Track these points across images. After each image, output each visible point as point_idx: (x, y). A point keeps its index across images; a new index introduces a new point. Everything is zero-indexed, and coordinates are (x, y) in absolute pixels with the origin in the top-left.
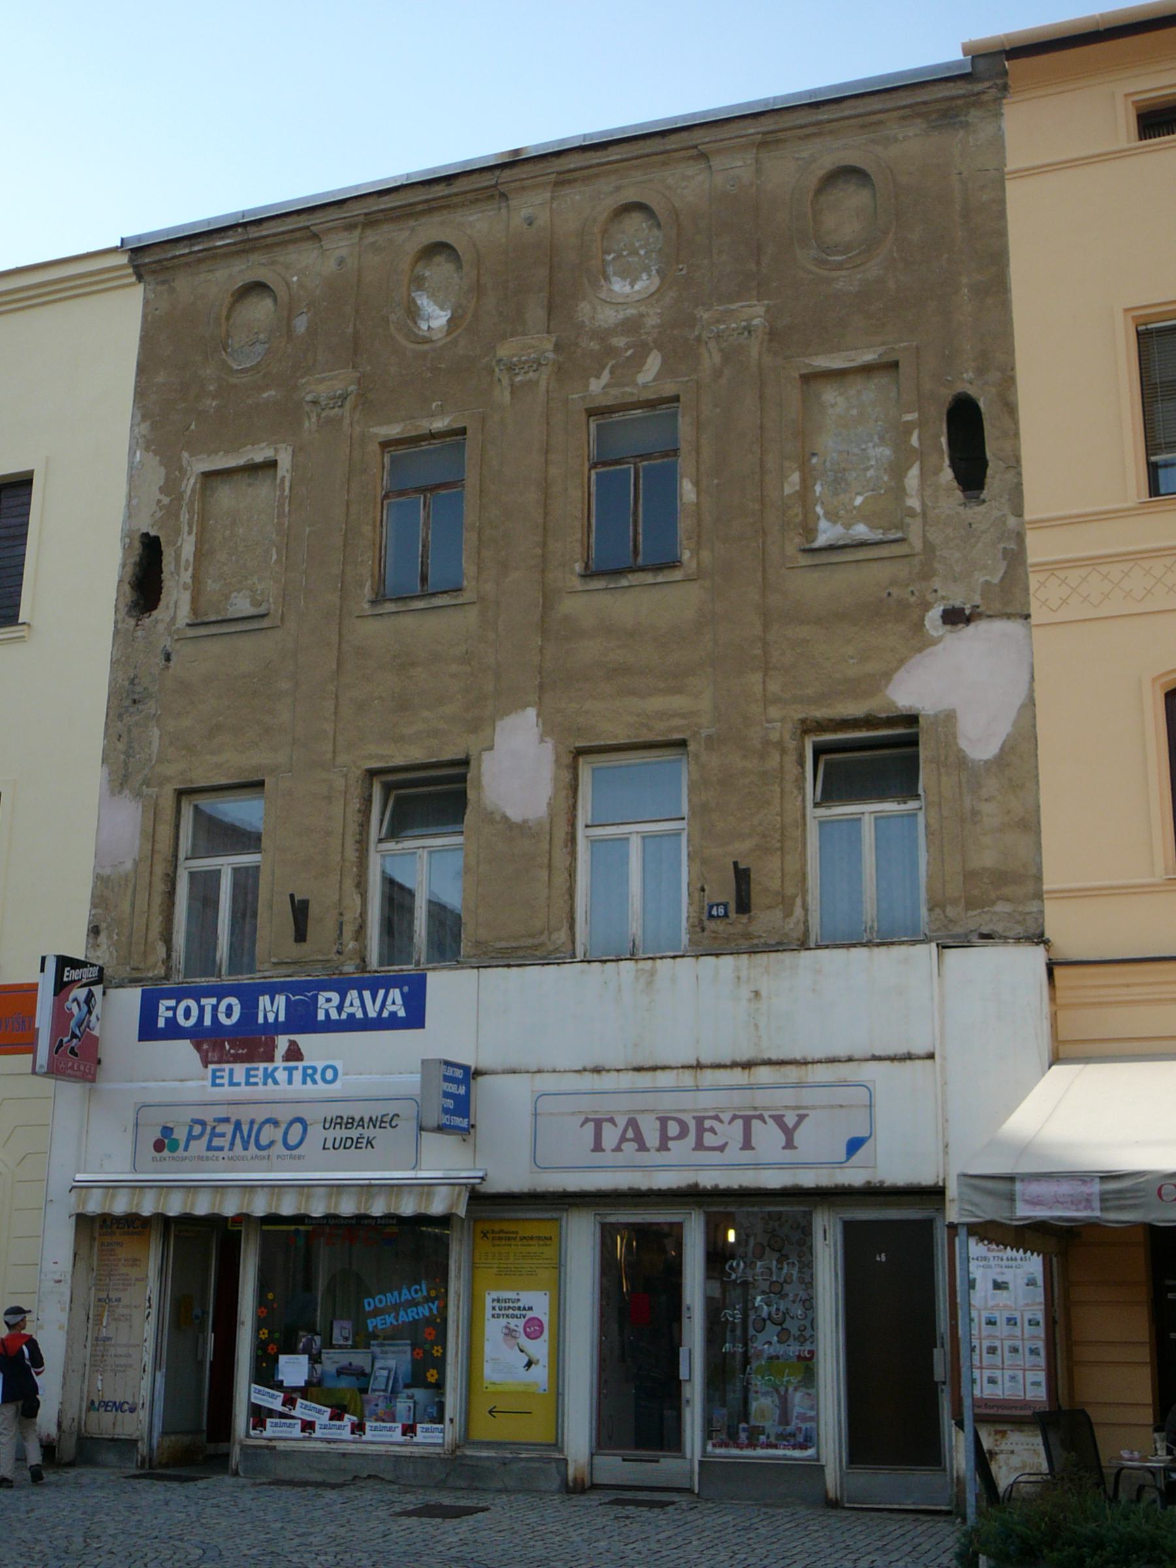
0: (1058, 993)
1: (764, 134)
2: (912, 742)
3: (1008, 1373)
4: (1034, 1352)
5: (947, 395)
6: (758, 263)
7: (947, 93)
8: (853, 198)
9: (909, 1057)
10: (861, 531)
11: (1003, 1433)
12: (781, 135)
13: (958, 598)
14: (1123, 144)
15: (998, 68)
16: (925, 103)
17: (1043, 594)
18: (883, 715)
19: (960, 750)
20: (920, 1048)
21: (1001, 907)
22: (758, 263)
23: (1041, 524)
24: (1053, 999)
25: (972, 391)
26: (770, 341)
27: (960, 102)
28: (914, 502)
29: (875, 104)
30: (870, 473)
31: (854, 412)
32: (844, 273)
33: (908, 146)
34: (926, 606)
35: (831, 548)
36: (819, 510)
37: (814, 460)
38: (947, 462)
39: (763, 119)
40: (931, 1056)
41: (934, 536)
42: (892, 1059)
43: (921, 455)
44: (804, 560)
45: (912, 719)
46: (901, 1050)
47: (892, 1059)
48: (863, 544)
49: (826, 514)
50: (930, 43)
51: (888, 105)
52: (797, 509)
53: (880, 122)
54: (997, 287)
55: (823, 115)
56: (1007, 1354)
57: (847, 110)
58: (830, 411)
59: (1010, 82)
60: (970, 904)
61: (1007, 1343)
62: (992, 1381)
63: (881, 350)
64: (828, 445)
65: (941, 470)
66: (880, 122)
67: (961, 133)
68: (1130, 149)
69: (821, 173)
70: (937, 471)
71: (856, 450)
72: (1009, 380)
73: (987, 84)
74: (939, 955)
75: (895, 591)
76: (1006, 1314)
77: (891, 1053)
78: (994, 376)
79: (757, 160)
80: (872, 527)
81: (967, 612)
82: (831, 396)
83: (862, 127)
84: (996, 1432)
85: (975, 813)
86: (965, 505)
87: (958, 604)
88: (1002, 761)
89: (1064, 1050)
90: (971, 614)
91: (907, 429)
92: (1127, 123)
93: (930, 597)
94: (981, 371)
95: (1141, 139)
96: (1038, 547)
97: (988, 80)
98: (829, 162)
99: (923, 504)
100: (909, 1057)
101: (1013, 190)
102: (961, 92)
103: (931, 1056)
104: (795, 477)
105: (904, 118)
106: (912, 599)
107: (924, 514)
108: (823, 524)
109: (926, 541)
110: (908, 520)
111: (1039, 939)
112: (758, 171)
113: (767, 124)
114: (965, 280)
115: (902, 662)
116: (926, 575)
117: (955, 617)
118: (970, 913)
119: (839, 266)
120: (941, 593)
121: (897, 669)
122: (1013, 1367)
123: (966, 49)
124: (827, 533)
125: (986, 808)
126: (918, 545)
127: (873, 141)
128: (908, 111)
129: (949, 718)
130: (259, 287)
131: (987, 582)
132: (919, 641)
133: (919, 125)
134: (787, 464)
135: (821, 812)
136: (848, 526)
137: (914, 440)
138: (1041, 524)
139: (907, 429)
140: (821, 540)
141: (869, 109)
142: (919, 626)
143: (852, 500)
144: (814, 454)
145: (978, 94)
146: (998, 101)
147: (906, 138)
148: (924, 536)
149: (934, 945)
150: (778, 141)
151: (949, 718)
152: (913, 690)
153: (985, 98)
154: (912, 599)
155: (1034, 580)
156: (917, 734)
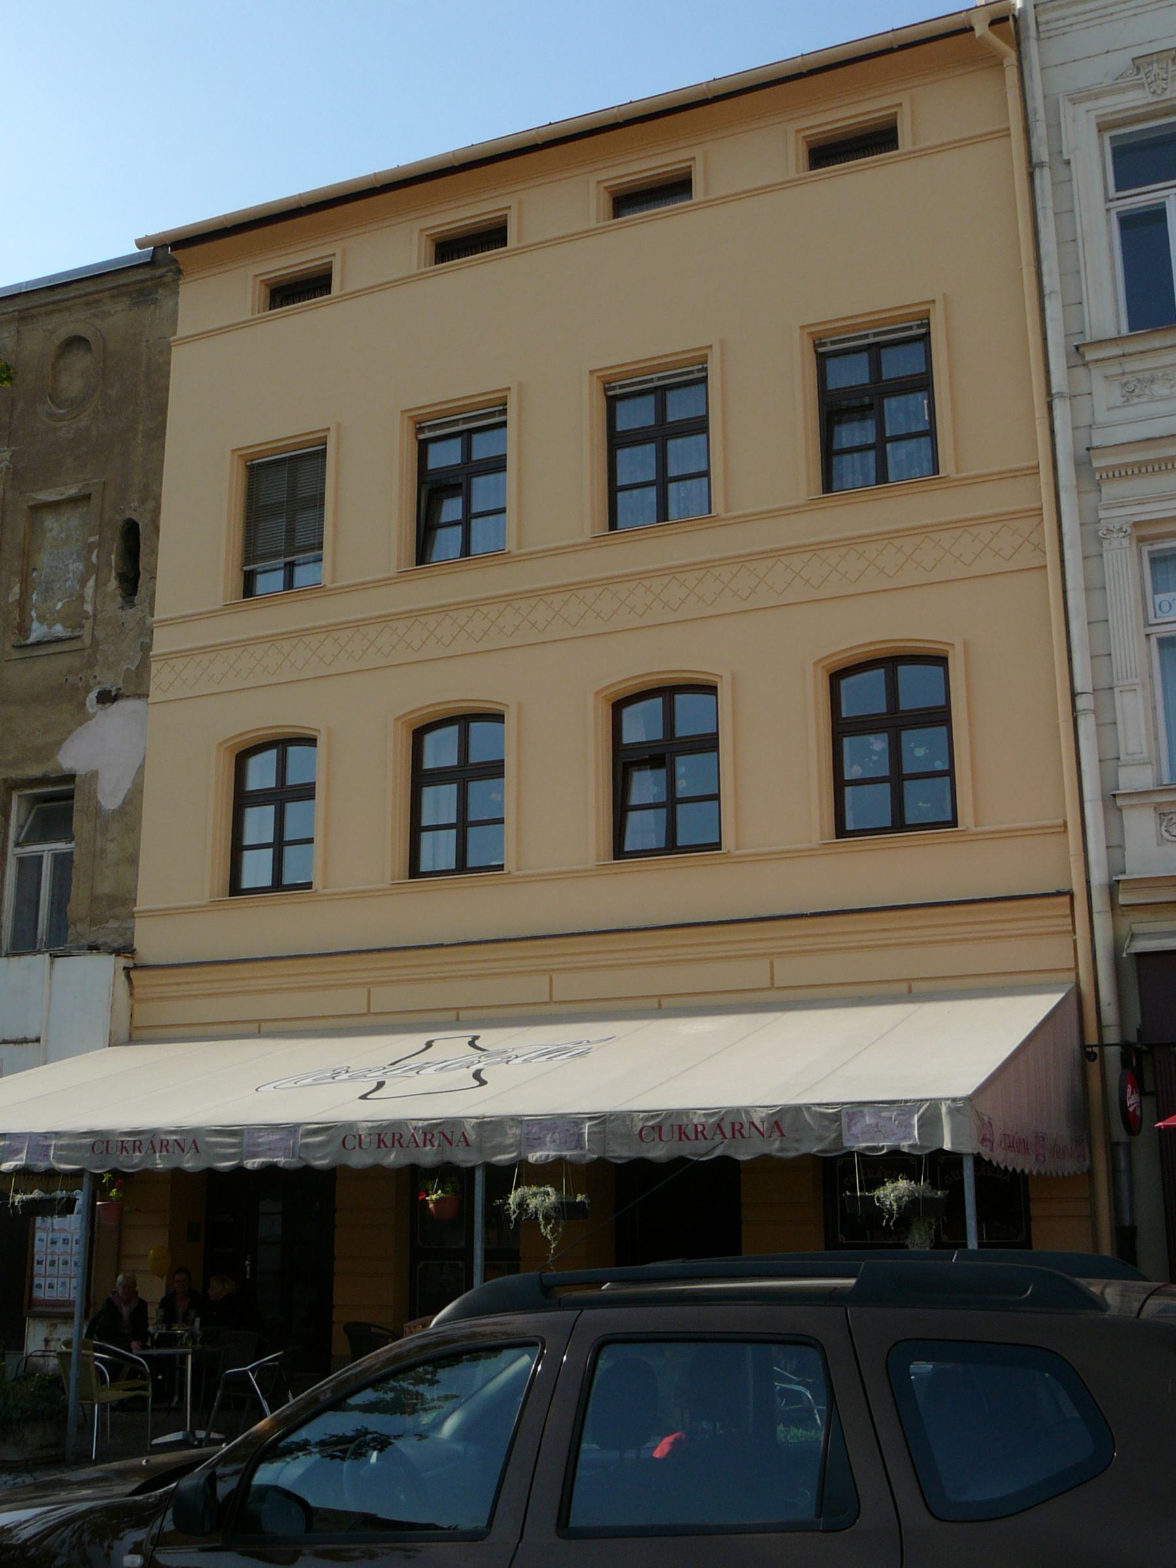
0: (136, 991)
1: (19, 311)
2: (69, 796)
3: (60, 1280)
4: (39, 1263)
5: (119, 519)
6: (11, 416)
7: (139, 277)
8: (80, 362)
9: (25, 1041)
10: (59, 630)
11: (55, 1326)
12: (33, 312)
13: (109, 681)
14: (793, 175)
15: (170, 259)
16: (125, 285)
17: (160, 677)
18: (53, 775)
19: (98, 802)
20: (32, 1035)
21: (113, 924)
22: (11, 416)
23: (164, 623)
24: (132, 994)
25: (135, 517)
26: (13, 479)
27: (149, 284)
28: (88, 608)
29: (91, 287)
30: (68, 584)
31: (63, 535)
32: (66, 423)
33: (118, 317)
34: (88, 689)
35: (38, 644)
36: (34, 614)
37: (35, 574)
38: (114, 574)
39: (17, 300)
40: (38, 1040)
41: (100, 635)
42: (15, 1042)
43: (96, 569)
44: (16, 655)
45: (70, 778)
46: (20, 1036)
47: (15, 1042)
48: (59, 640)
49: (38, 616)
50: (113, 241)
51: (100, 287)
52: (16, 614)
53: (98, 301)
54: (158, 434)
55: (59, 296)
56: (61, 1266)
57: (73, 292)
58: (49, 534)
59: (182, 267)
60: (93, 922)
61: (62, 1258)
62: (51, 1286)
63: (80, 485)
64: (45, 561)
65: (109, 580)
66: (98, 301)
67: (152, 307)
68: (801, 179)
69: (58, 342)
70: (108, 581)
71: (61, 566)
72: (157, 510)
73: (165, 269)
74: (52, 963)
75: (70, 678)
76: (63, 1235)
77: (14, 1038)
78: (150, 505)
79: (19, 332)
80: (65, 627)
81: (113, 693)
82: (52, 525)
83: (87, 304)
84: (52, 1325)
85: (103, 851)
86: (122, 608)
87: (107, 686)
88: (122, 811)
89: (137, 1034)
90: (116, 695)
91: (90, 548)
92: (796, 154)
93: (92, 682)
94: (143, 501)
95: (811, 169)
96: (161, 642)
97: (165, 265)
98: (64, 333)
99: (95, 608)
100: (25, 1041)
101: (179, 357)
102: (148, 276)
103: (38, 1040)
104: (17, 589)
105: (113, 297)
106: (80, 684)
107: (95, 616)
108: (35, 625)
109: (93, 638)
110: (84, 621)
111: (125, 950)
112: (19, 340)
113: (20, 304)
114: (141, 427)
115: (70, 733)
116: (91, 664)
117: (106, 698)
118: (94, 929)
119: (61, 418)
120: (98, 679)
121: (64, 740)
122: (64, 1275)
123: (140, 244)
124: (38, 631)
125: (111, 846)
126: (87, 641)
127: (95, 316)
128: (114, 292)
129: (93, 776)
130: (76, 342)
131: (128, 669)
132: (81, 717)
133: (121, 305)
134: (13, 578)
135: (19, 850)
136: (50, 626)
137: (94, 559)
138: (164, 623)
139: (90, 548)
140: (33, 638)
141: (88, 290)
142: (82, 705)
143: (55, 605)
144: (34, 570)
145: (160, 277)
146: (176, 281)
147: (116, 312)
148: (93, 634)
149: (47, 955)
150: (33, 316)
151: (93, 776)
152: (73, 757)
153: (166, 280)
154: (80, 684)
155: (154, 667)
156: (73, 791)
